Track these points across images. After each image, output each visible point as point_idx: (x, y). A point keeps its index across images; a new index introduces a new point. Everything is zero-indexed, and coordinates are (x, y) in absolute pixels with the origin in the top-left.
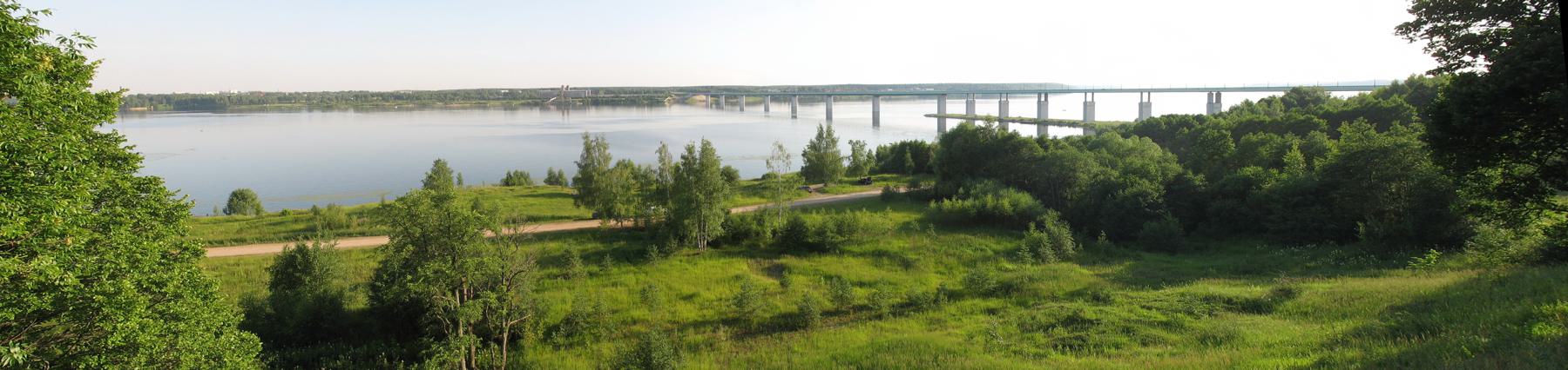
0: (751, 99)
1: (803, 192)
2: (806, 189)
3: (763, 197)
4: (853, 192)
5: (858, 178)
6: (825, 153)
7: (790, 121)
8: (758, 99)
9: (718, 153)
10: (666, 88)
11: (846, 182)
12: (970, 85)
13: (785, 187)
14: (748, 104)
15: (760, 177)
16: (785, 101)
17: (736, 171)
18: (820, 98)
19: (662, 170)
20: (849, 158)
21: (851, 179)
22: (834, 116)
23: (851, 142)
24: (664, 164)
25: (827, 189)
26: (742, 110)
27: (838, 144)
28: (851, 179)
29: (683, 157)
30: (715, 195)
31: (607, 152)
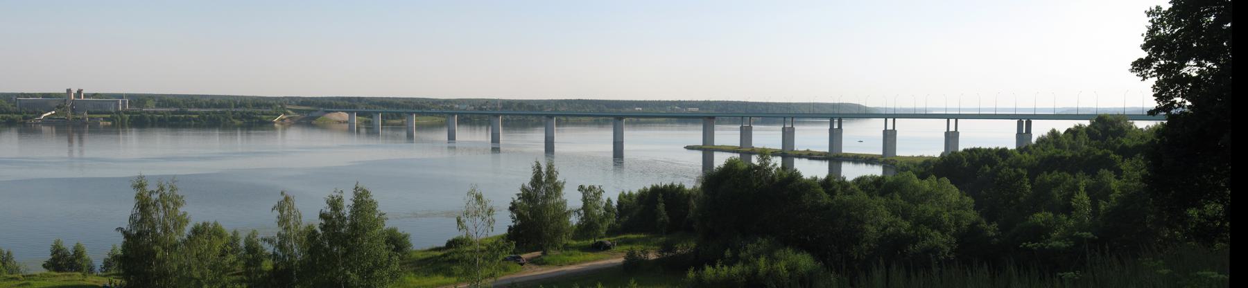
0: (425, 120)
1: (512, 265)
2: (516, 259)
5: (592, 241)
6: (544, 205)
7: (489, 157)
8: (438, 120)
9: (381, 208)
10: (277, 99)
11: (574, 248)
14: (420, 127)
15: (443, 244)
16: (481, 124)
17: (405, 236)
19: (283, 239)
23: (581, 188)
25: (546, 258)
26: (410, 137)
29: (322, 216)
30: (376, 273)
31: (181, 210)
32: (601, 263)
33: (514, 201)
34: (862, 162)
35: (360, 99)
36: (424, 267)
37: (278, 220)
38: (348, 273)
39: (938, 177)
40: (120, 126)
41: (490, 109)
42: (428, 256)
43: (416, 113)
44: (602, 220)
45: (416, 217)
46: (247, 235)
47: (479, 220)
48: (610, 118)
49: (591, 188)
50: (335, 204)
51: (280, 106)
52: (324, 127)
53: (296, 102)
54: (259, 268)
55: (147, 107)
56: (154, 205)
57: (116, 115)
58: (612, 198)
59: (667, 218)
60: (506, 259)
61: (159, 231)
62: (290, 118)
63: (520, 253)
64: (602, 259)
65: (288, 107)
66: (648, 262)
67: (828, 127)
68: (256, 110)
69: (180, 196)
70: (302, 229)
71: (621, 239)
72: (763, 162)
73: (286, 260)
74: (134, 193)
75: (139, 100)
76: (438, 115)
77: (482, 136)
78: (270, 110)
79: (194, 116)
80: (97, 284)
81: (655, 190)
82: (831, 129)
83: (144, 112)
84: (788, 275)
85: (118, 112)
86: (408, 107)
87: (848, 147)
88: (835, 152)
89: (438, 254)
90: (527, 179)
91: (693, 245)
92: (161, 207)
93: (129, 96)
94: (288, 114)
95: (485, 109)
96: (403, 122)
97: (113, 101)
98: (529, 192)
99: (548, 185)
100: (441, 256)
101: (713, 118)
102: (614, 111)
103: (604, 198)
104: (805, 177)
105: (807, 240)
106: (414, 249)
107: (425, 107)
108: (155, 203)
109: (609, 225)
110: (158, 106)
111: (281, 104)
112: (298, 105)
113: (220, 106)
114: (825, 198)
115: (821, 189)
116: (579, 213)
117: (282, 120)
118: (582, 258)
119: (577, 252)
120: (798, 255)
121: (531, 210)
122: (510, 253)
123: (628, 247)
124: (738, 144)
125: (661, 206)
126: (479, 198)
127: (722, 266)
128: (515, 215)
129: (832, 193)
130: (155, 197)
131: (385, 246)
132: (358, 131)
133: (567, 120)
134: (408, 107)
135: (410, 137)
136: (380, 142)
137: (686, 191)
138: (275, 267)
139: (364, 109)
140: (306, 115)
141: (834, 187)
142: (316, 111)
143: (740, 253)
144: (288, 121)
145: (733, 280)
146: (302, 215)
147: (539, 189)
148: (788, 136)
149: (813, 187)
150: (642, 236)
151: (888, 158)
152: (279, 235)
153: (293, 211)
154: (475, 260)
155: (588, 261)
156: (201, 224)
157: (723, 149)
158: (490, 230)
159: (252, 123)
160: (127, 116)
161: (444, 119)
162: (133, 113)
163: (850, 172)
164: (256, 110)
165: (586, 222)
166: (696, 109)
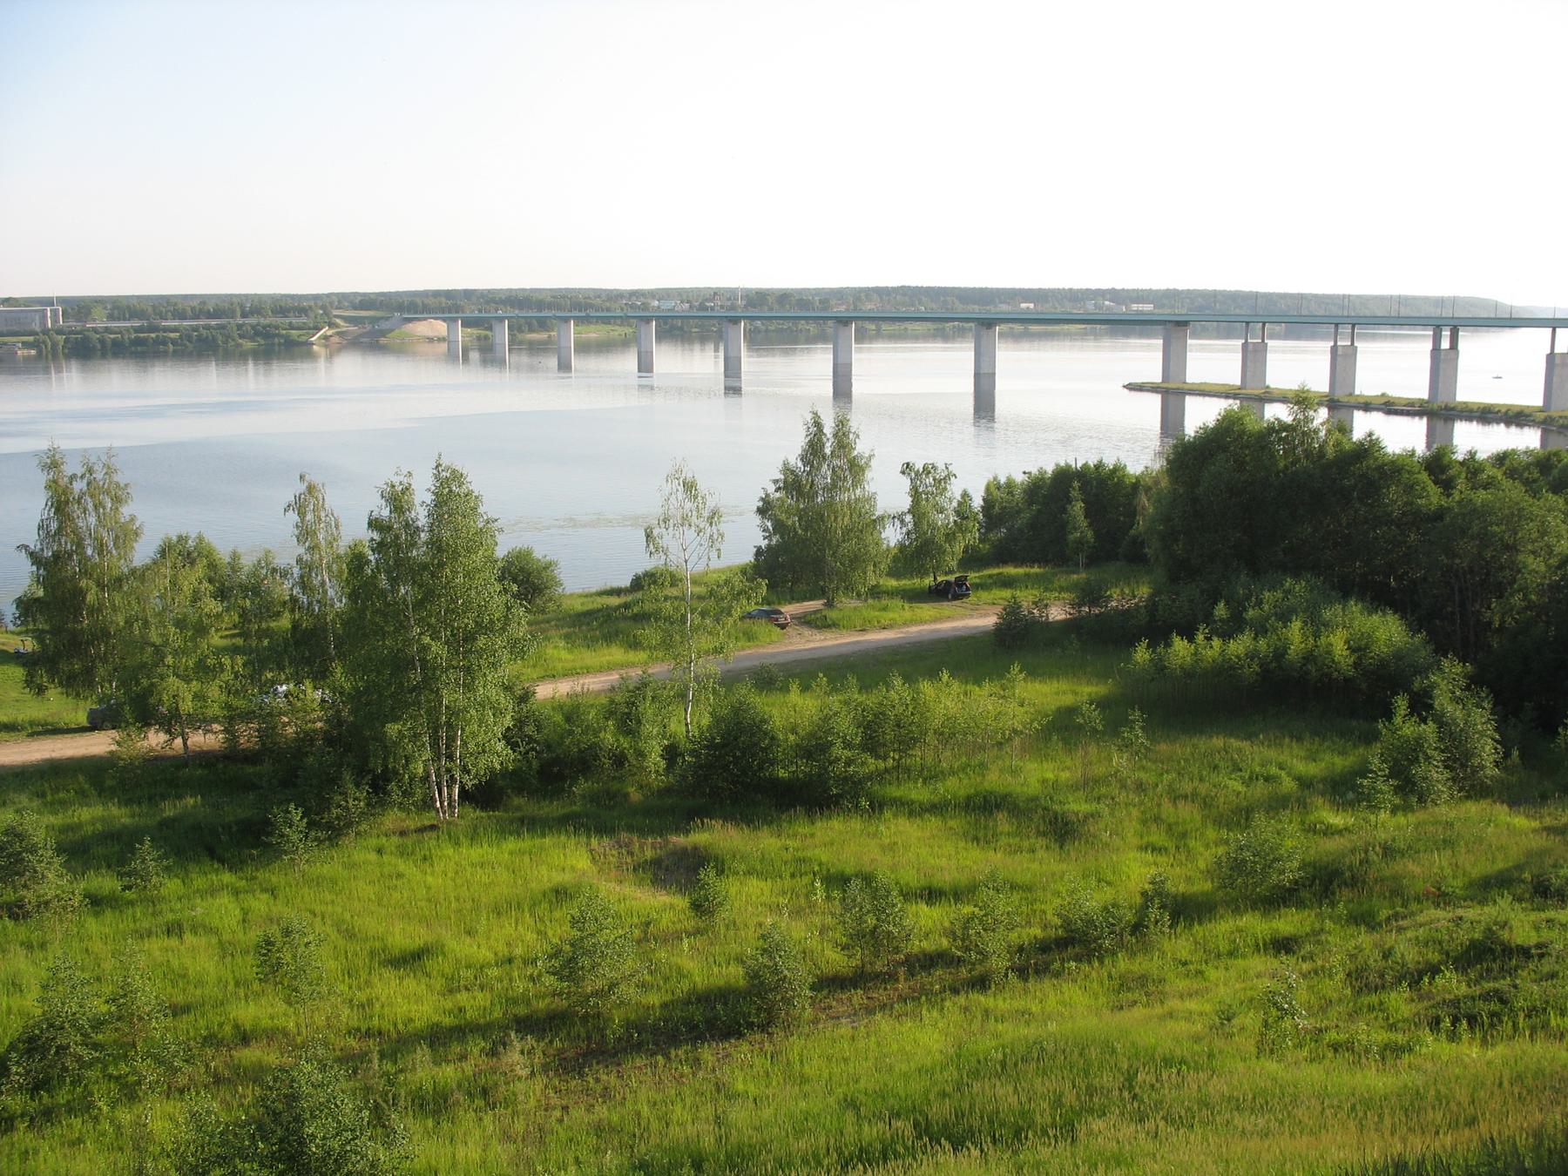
0: (594, 333)
1: (762, 628)
2: (771, 616)
3: (635, 645)
5: (928, 581)
6: (830, 504)
7: (721, 402)
8: (618, 331)
9: (487, 509)
10: (316, 297)
11: (892, 594)
13: (703, 614)
14: (584, 348)
15: (625, 582)
16: (703, 339)
17: (548, 566)
18: (812, 328)
19: (307, 568)
22: (858, 388)
23: (907, 468)
25: (833, 615)
26: (564, 366)
27: (869, 475)
29: (374, 524)
30: (481, 641)
31: (126, 511)
32: (946, 626)
33: (767, 495)
34: (1498, 421)
35: (468, 294)
36: (584, 628)
37: (297, 532)
38: (427, 640)
39: (909, 679)
40: (50, 356)
41: (722, 307)
42: (595, 606)
43: (575, 318)
44: (950, 537)
45: (574, 526)
46: (255, 560)
47: (691, 534)
48: (967, 325)
49: (927, 470)
50: (397, 499)
51: (321, 312)
52: (400, 349)
53: (351, 302)
54: (1356, 589)
55: (94, 320)
56: (79, 503)
57: (42, 337)
58: (970, 492)
59: (1090, 534)
60: (750, 616)
61: (89, 552)
62: (340, 334)
63: (779, 603)
64: (949, 618)
65: (336, 312)
66: (1049, 626)
67: (1429, 345)
68: (279, 320)
69: (122, 485)
70: (342, 551)
71: (990, 576)
72: (1301, 416)
73: (313, 610)
74: (42, 478)
75: (79, 308)
76: (619, 322)
77: (704, 364)
78: (304, 320)
79: (172, 335)
80: (5, 648)
81: (1065, 477)
82: (1436, 349)
83: (88, 330)
84: (1351, 661)
85: (46, 332)
86: (302, 311)
87: (1468, 391)
88: (1442, 399)
89: (614, 601)
90: (791, 448)
91: (1144, 591)
92: (90, 506)
93: (63, 301)
94: (337, 326)
95: (712, 309)
96: (550, 337)
97: (36, 311)
98: (797, 476)
99: (836, 462)
100: (619, 607)
101: (1185, 324)
102: (976, 310)
103: (955, 490)
104: (1390, 450)
105: (1388, 585)
106: (568, 592)
107: (591, 306)
108: (80, 498)
109: (966, 547)
110: (111, 317)
111: (323, 308)
112: (355, 308)
113: (217, 314)
114: (1433, 497)
115: (1424, 476)
116: (902, 521)
117: (326, 338)
118: (907, 614)
119: (898, 602)
120: (1375, 617)
121: (802, 514)
122: (757, 604)
123: (1007, 593)
124: (1423, 394)
125: (1078, 508)
126: (690, 487)
127: (1209, 639)
128: (769, 524)
129: (1447, 486)
130: (79, 486)
131: (498, 587)
132: (466, 359)
133: (878, 330)
134: (560, 308)
135: (564, 366)
136: (507, 376)
137: (1128, 476)
138: (296, 626)
139: (476, 314)
140: (368, 327)
141: (1452, 472)
142: (387, 319)
143: (1245, 609)
144: (336, 339)
145: (1232, 668)
146: (341, 521)
147: (819, 469)
148: (1342, 363)
149: (1409, 472)
150: (1036, 570)
151: (1555, 414)
152: (299, 561)
153: (323, 514)
154: (684, 617)
155: (922, 622)
156: (175, 539)
157: (1203, 391)
158: (714, 554)
159: (273, 344)
160: (61, 338)
161: (629, 330)
162: (71, 332)
163: (1472, 440)
164: (279, 320)
165: (916, 540)
166: (1148, 307)
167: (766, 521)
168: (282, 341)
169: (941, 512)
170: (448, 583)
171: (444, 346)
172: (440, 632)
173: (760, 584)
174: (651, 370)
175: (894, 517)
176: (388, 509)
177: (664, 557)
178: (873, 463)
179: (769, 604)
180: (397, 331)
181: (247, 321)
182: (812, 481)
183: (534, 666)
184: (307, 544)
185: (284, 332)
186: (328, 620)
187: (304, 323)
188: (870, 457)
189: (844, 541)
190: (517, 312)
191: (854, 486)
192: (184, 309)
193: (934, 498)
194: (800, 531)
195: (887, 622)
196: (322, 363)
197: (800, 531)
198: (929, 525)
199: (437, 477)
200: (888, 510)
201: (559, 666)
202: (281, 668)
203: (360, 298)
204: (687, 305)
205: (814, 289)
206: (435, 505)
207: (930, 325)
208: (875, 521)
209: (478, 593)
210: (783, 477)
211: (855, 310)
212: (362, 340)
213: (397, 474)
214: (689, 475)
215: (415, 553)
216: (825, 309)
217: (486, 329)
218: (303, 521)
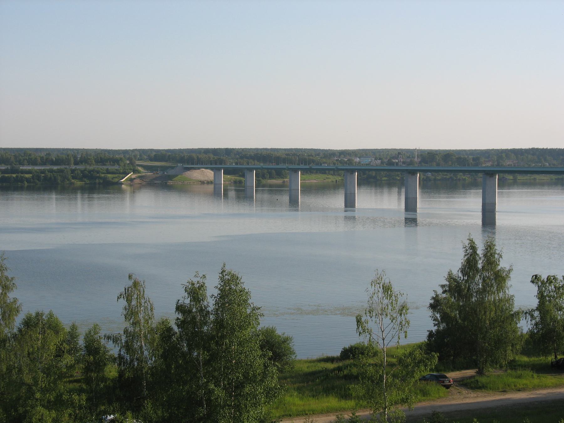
0: (315, 179)
1: (433, 387)
2: (440, 379)
3: (346, 396)
4: (535, 388)
5: (551, 358)
6: (481, 303)
7: (402, 230)
8: (331, 179)
9: (255, 300)
10: (125, 152)
11: (524, 366)
12: (257, 149)
13: (395, 376)
14: (308, 189)
15: (337, 353)
16: (390, 184)
17: (286, 340)
18: (467, 178)
19: (131, 336)
20: (530, 313)
21: (534, 359)
22: (501, 220)
23: (536, 279)
24: (134, 324)
25: (483, 380)
26: (294, 203)
27: (509, 283)
28: (534, 359)
29: (180, 308)
30: (247, 389)
31: (11, 295)
35: (228, 152)
37: (125, 313)
38: (212, 386)
41: (404, 163)
43: (301, 169)
47: (387, 321)
51: (128, 162)
53: (149, 156)
60: (424, 379)
62: (141, 177)
63: (445, 371)
65: (138, 162)
69: (10, 278)
70: (154, 326)
73: (134, 365)
76: (332, 172)
78: (116, 167)
79: (27, 176)
86: (116, 161)
89: (330, 366)
94: (139, 172)
95: (397, 164)
96: (284, 182)
98: (458, 282)
99: (486, 274)
100: (334, 370)
106: (298, 358)
107: (313, 161)
111: (130, 159)
112: (151, 160)
113: (58, 162)
116: (532, 316)
117: (131, 180)
118: (536, 381)
119: (529, 373)
121: (461, 309)
122: (431, 370)
126: (387, 289)
131: (260, 353)
132: (226, 195)
134: (291, 162)
135: (294, 203)
138: (121, 374)
139: (234, 165)
140: (160, 173)
142: (172, 168)
144: (137, 181)
146: (155, 306)
147: (473, 278)
152: (126, 331)
153: (143, 301)
154: (381, 377)
155: (546, 387)
158: (402, 335)
161: (339, 178)
165: (542, 329)
167: (436, 314)
168: (101, 181)
169: (560, 310)
170: (227, 349)
171: (211, 187)
172: (220, 382)
173: (434, 356)
174: (353, 206)
175: (526, 313)
176: (189, 299)
177: (368, 336)
178: (512, 275)
179: (438, 371)
180: (179, 176)
181: (78, 167)
182: (469, 287)
183: (277, 408)
184: (131, 321)
185: (103, 175)
186: (144, 372)
187: (117, 170)
188: (510, 271)
189: (491, 329)
190: (262, 164)
191: (498, 291)
192: (36, 158)
193: (555, 300)
194: (460, 321)
195: (522, 386)
196: (128, 196)
197: (460, 321)
198: (551, 319)
199: (222, 279)
200: (521, 307)
201: (294, 408)
202: (110, 403)
203: (154, 153)
204: (379, 161)
205: (469, 150)
206: (220, 297)
207: (553, 177)
208: (512, 315)
209: (246, 357)
210: (448, 283)
211: (498, 165)
212: (156, 182)
213: (196, 276)
214: (387, 281)
215: (206, 328)
216: (477, 165)
217: (240, 176)
218: (129, 305)
